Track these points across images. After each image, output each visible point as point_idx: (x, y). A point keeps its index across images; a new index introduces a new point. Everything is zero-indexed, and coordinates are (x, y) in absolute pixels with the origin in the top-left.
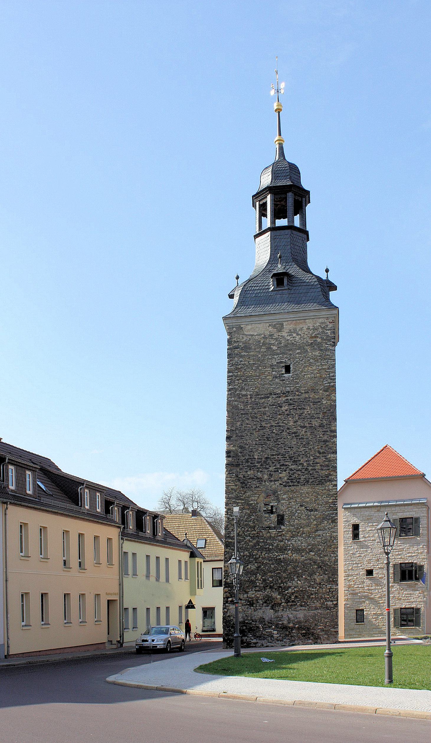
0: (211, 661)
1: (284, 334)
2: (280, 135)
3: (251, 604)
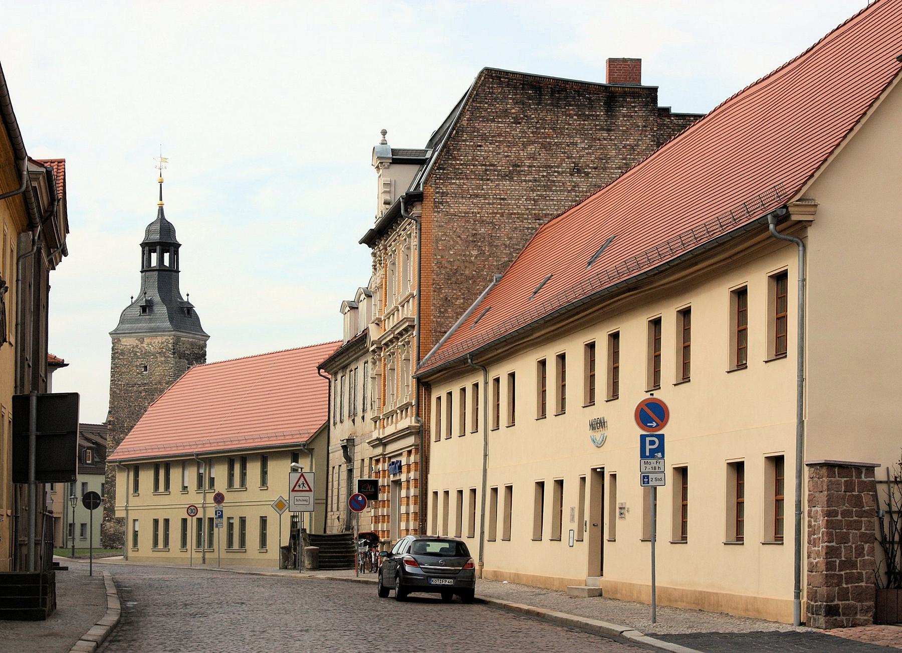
0: (835, 630)
1: (145, 345)
2: (161, 199)
3: (119, 522)
